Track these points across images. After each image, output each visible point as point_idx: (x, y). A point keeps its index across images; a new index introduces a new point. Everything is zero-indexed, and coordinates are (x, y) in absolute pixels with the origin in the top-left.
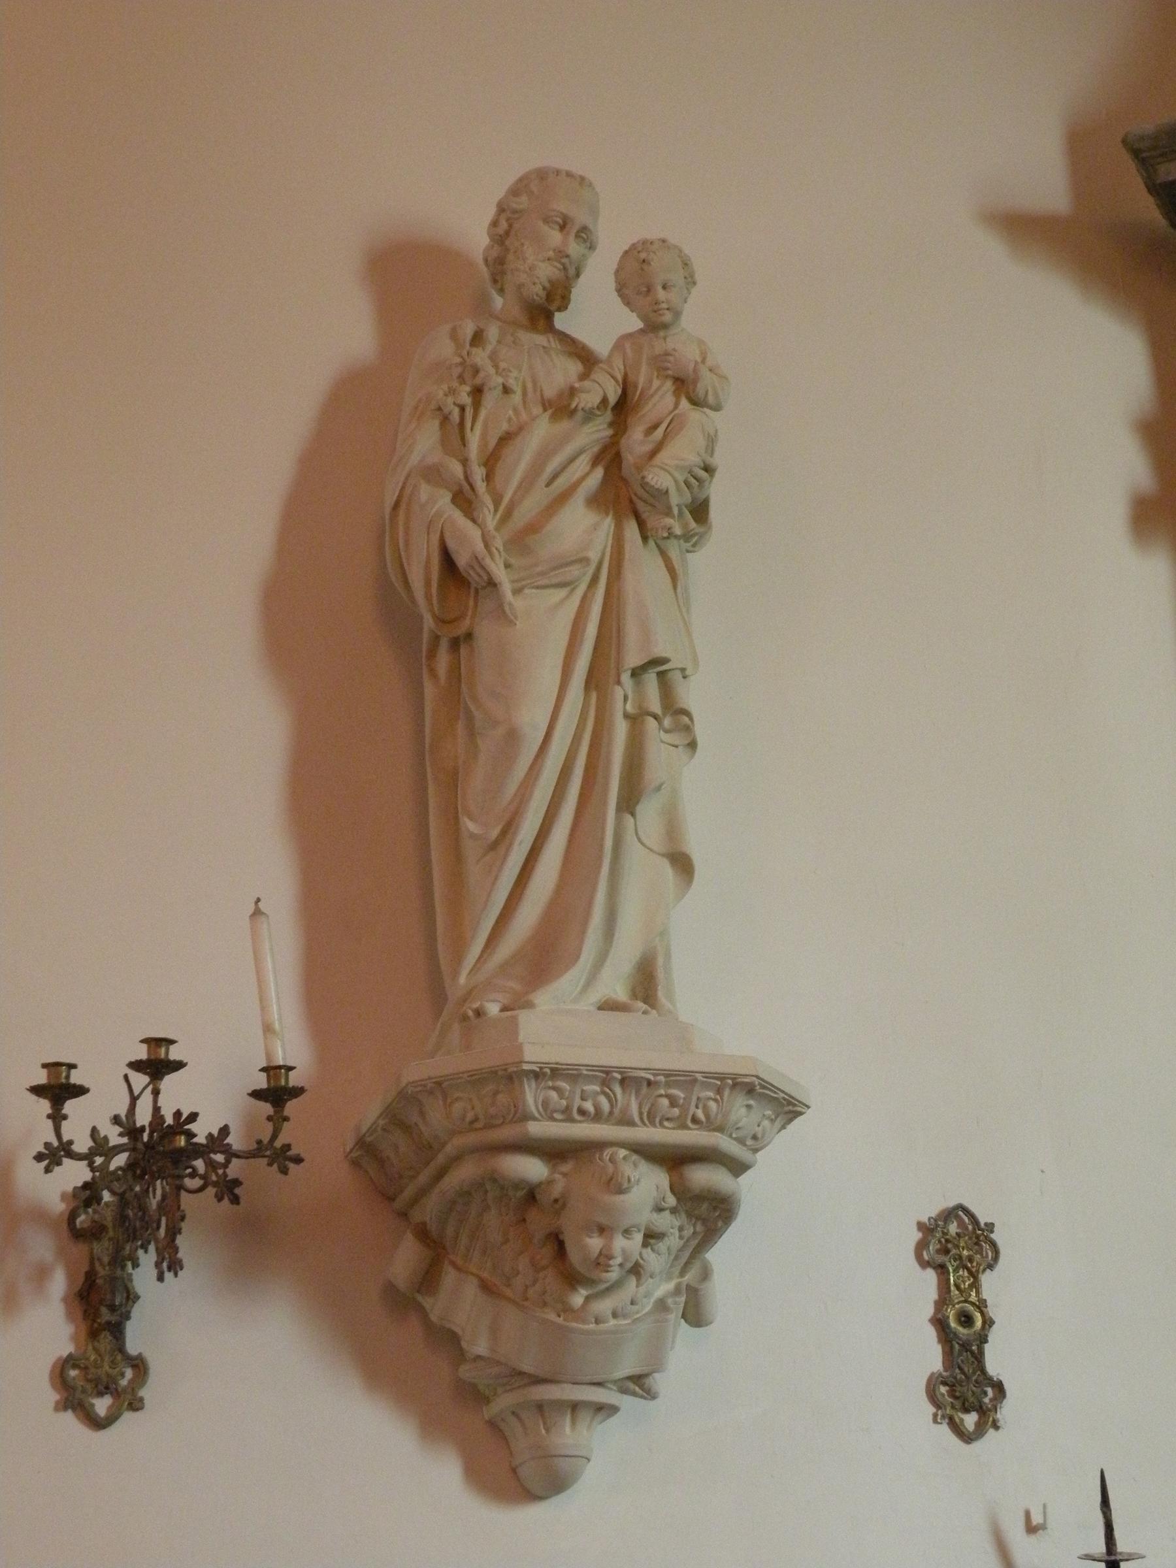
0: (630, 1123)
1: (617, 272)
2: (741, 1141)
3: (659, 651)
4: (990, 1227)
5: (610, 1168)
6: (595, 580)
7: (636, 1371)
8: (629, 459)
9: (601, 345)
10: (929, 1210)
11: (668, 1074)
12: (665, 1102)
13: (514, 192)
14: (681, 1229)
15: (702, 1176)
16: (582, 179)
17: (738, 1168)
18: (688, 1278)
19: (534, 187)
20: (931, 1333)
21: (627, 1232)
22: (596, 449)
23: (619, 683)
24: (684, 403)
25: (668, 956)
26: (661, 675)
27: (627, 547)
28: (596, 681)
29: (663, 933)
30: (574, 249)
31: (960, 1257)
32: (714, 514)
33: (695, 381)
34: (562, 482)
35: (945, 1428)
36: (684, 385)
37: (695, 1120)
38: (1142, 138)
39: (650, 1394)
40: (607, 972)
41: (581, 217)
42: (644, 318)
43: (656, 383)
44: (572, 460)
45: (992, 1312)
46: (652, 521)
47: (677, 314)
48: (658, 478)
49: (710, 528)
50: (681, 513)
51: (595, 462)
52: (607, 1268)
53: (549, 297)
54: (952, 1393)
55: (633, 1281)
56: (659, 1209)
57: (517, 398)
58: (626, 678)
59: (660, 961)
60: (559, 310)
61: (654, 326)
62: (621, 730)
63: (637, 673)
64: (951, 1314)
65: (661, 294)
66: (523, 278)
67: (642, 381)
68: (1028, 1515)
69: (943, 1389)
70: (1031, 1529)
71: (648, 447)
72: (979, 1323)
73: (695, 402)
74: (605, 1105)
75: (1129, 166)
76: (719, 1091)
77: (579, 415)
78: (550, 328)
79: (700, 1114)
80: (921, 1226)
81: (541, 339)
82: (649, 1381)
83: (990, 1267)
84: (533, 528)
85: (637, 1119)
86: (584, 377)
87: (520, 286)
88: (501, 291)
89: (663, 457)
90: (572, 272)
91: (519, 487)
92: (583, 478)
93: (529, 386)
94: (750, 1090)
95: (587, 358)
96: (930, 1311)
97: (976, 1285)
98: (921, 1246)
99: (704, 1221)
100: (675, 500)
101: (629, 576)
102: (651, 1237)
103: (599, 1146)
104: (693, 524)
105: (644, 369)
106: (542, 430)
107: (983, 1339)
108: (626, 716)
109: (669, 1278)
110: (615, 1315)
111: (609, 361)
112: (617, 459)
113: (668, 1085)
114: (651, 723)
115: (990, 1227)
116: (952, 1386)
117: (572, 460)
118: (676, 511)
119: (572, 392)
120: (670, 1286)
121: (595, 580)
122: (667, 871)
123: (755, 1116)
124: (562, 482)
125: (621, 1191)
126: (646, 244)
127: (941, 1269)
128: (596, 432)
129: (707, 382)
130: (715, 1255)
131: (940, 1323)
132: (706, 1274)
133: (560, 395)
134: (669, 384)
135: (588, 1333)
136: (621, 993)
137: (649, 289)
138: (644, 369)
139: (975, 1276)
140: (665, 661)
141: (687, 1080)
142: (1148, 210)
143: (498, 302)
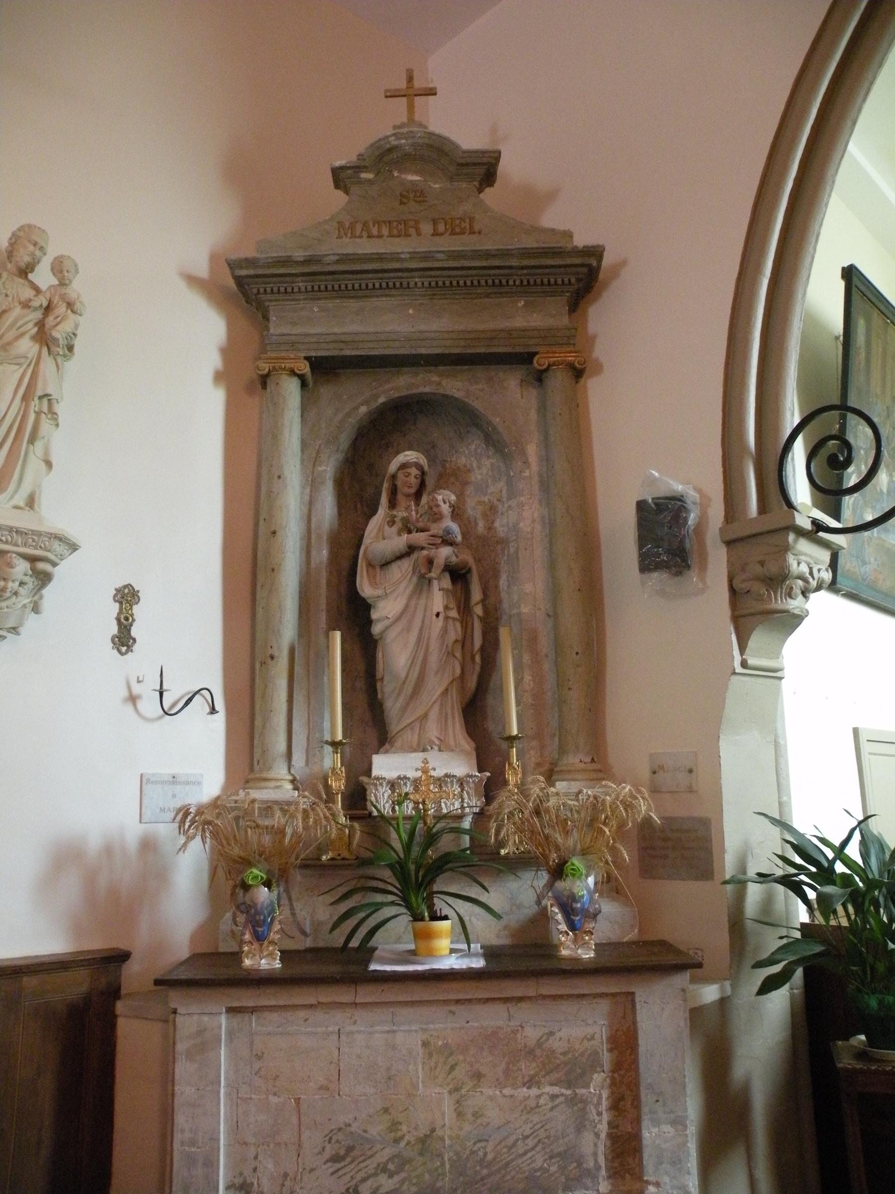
0: (18, 546)
1: (52, 264)
2: (56, 555)
3: (49, 391)
4: (138, 591)
5: (9, 560)
6: (29, 365)
7: (14, 625)
8: (47, 326)
9: (43, 287)
10: (120, 585)
11: (32, 531)
12: (30, 540)
13: (19, 229)
14: (33, 582)
15: (41, 566)
16: (44, 231)
17: (54, 564)
18: (35, 598)
19: (26, 229)
20: (115, 622)
21: (13, 581)
22: (36, 321)
23: (33, 400)
24: (69, 311)
25: (40, 494)
26: (49, 400)
27: (43, 356)
28: (26, 398)
29: (39, 486)
30: (38, 253)
31: (127, 600)
32: (76, 349)
33: (74, 304)
34: (22, 330)
35: (115, 651)
36: (70, 305)
37: (40, 547)
38: (231, 260)
39: (18, 634)
40: (17, 497)
41: (41, 243)
42: (59, 281)
43: (61, 303)
44: (26, 323)
45: (135, 617)
46: (53, 348)
47: (71, 282)
48: (56, 334)
49: (74, 354)
50: (63, 347)
51: (36, 325)
52: (5, 592)
53: (27, 267)
54: (119, 641)
55: (15, 597)
56: (26, 575)
57: (10, 299)
58: (36, 399)
59: (37, 495)
60: (31, 272)
61: (62, 284)
62: (32, 417)
63: (40, 398)
64: (122, 617)
65: (66, 274)
66: (18, 259)
67: (55, 302)
68: (138, 677)
69: (117, 639)
70: (139, 682)
71: (55, 323)
72: (130, 620)
73: (73, 312)
74: (9, 538)
75: (227, 270)
76: (50, 538)
77: (31, 309)
78: (26, 278)
79: (42, 545)
80: (116, 590)
81: (21, 281)
82: (18, 629)
83: (137, 603)
84: (9, 343)
85: (20, 543)
86: (36, 296)
87: (17, 262)
88: (11, 262)
89: (59, 327)
90: (36, 261)
91: (7, 329)
92: (30, 330)
93: (15, 296)
94: (60, 539)
95: (38, 290)
96: (116, 615)
97: (131, 609)
98: (115, 596)
99: (42, 580)
100: (61, 342)
101: (42, 366)
102: (22, 584)
103: (7, 552)
104: (67, 352)
105: (57, 297)
106: (17, 311)
107: (131, 625)
108: (35, 412)
109: (29, 598)
110: (7, 607)
111: (45, 292)
112: (44, 325)
113: (33, 534)
114: (43, 416)
115: (138, 591)
116: (119, 638)
117: (26, 323)
118: (61, 346)
119: (30, 300)
120: (28, 600)
121: (29, 365)
122: (43, 465)
123: (62, 548)
124: (22, 330)
125: (12, 567)
126: (62, 256)
127: (121, 603)
128: (39, 315)
129: (78, 306)
130: (45, 592)
131: (118, 620)
132: (41, 598)
133: (26, 300)
134: (65, 304)
135: (6, 613)
136: (22, 504)
137: (61, 272)
138: (57, 297)
139: (131, 606)
140: (51, 395)
141: (39, 534)
142: (231, 283)
143: (9, 266)
